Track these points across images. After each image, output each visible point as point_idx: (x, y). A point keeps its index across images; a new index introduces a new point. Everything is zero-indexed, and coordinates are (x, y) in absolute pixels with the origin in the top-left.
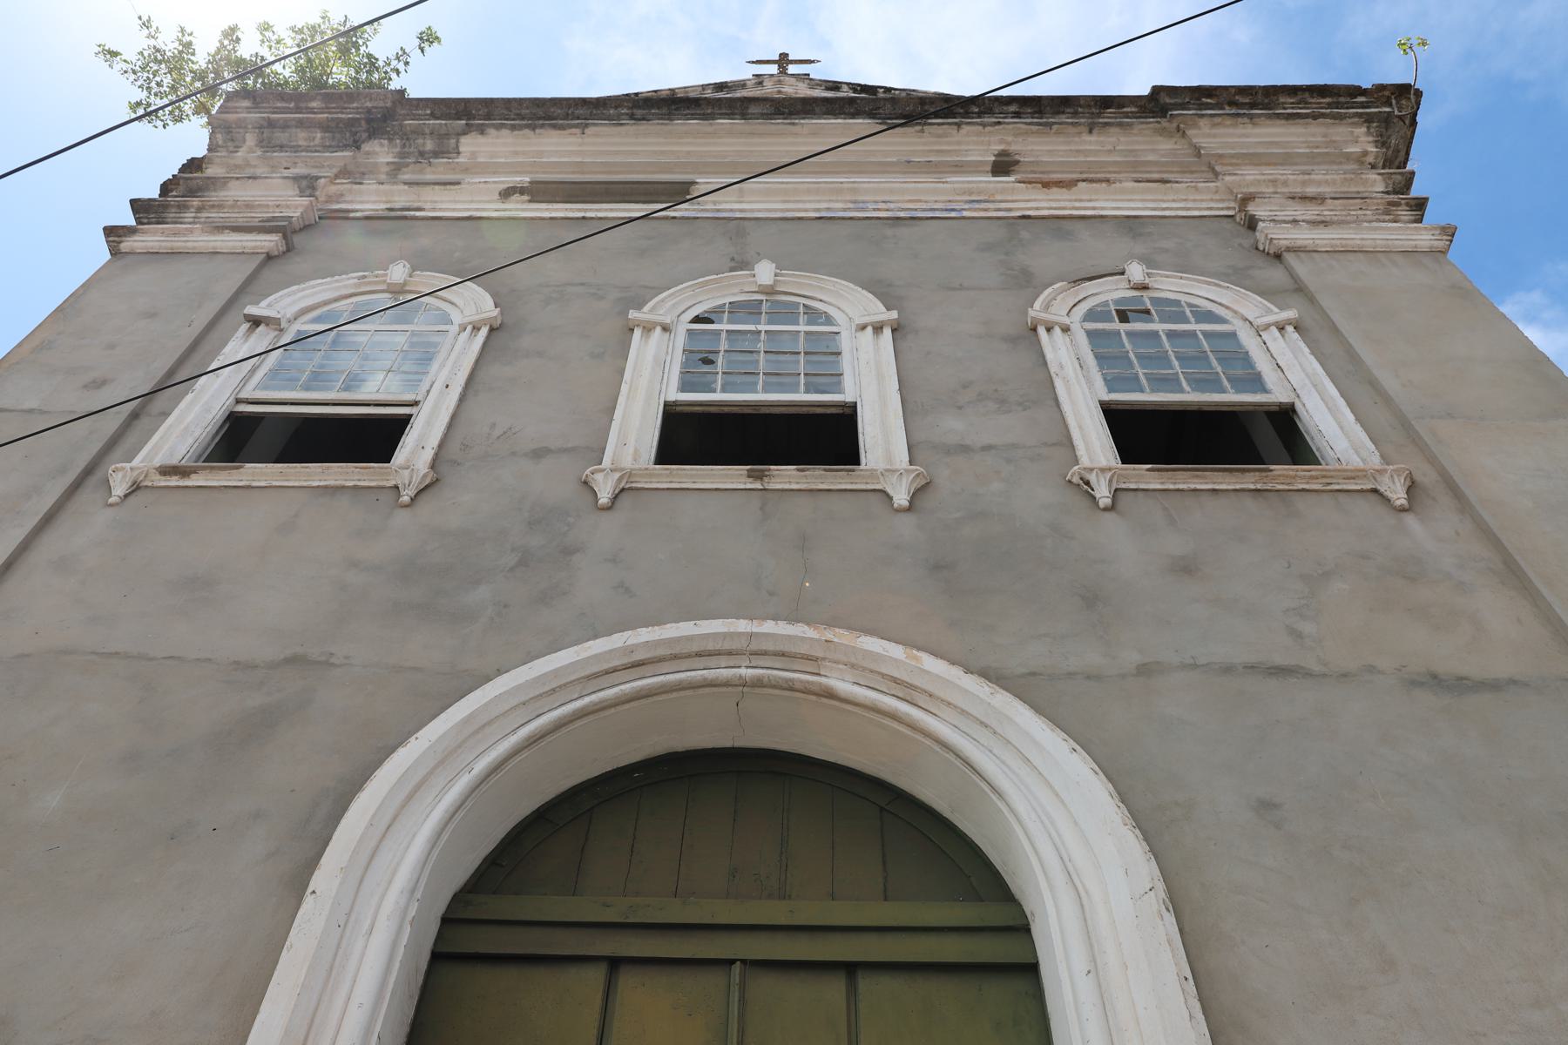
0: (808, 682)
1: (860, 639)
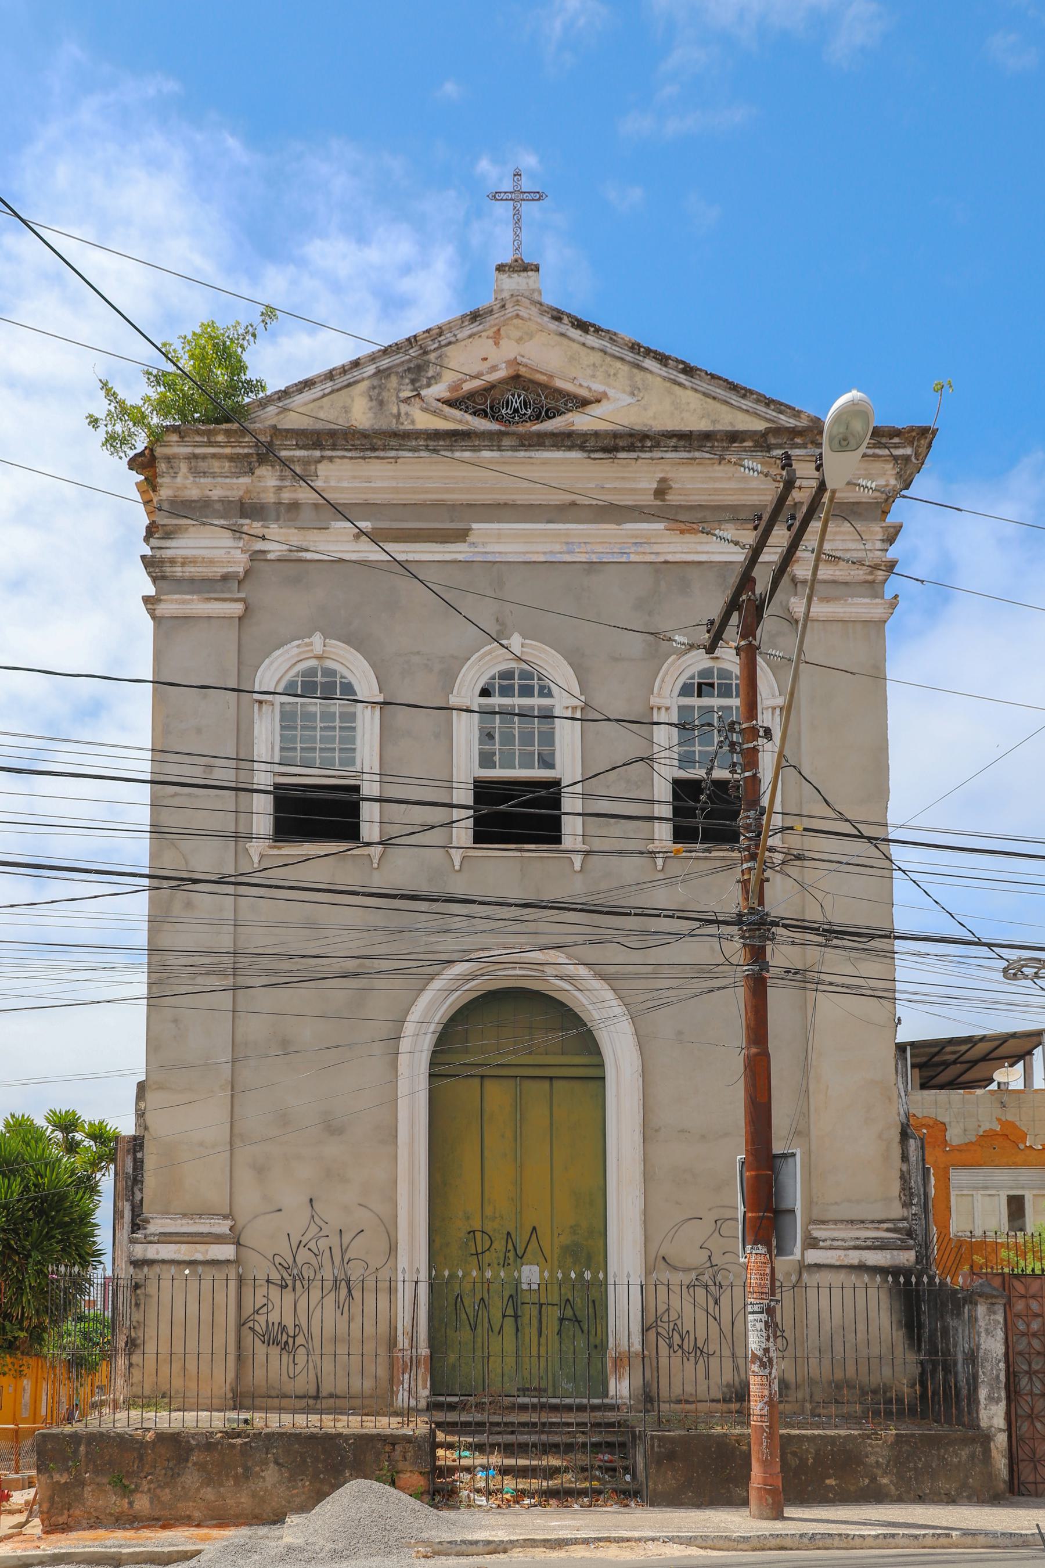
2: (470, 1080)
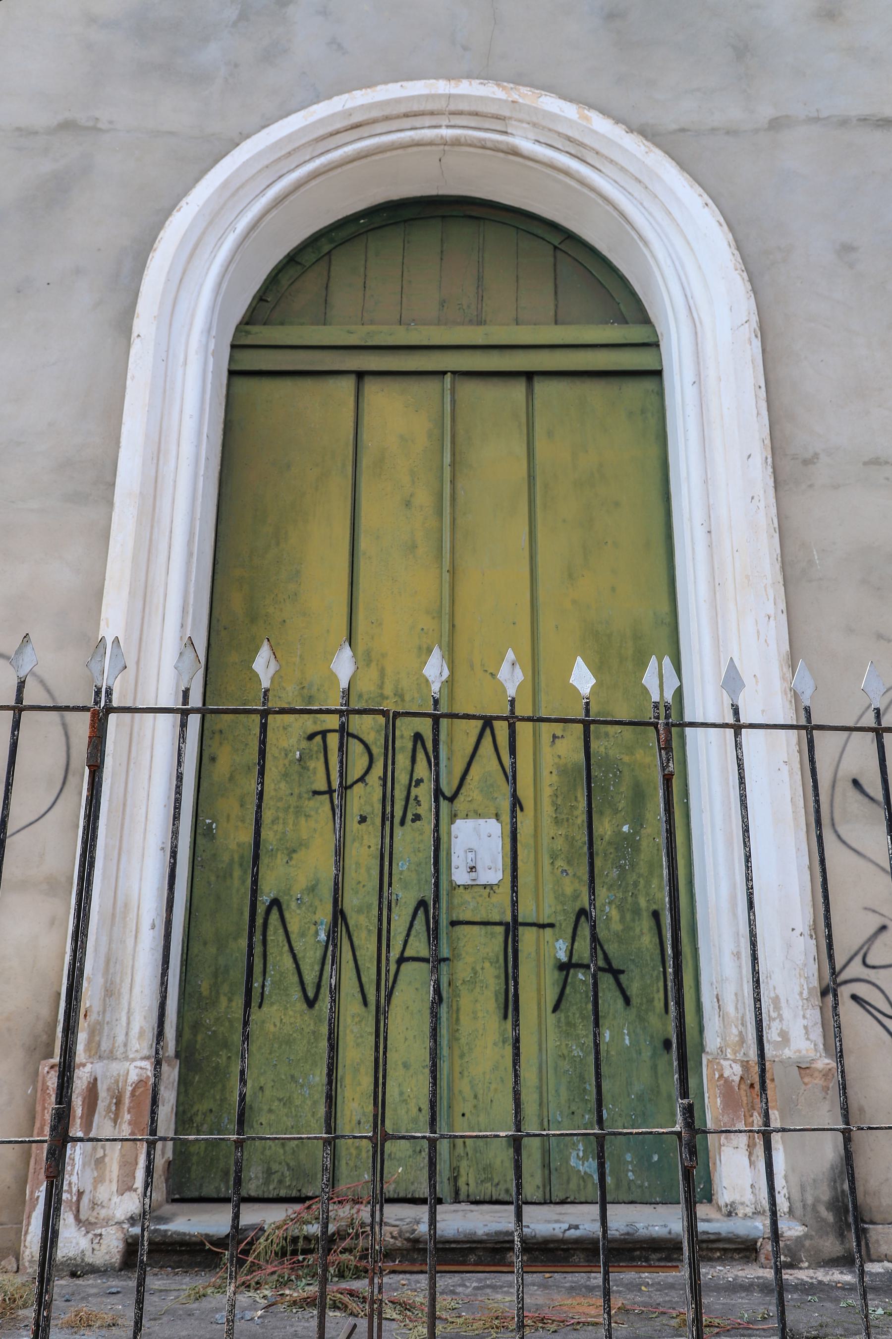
0: (498, 142)
1: (541, 99)
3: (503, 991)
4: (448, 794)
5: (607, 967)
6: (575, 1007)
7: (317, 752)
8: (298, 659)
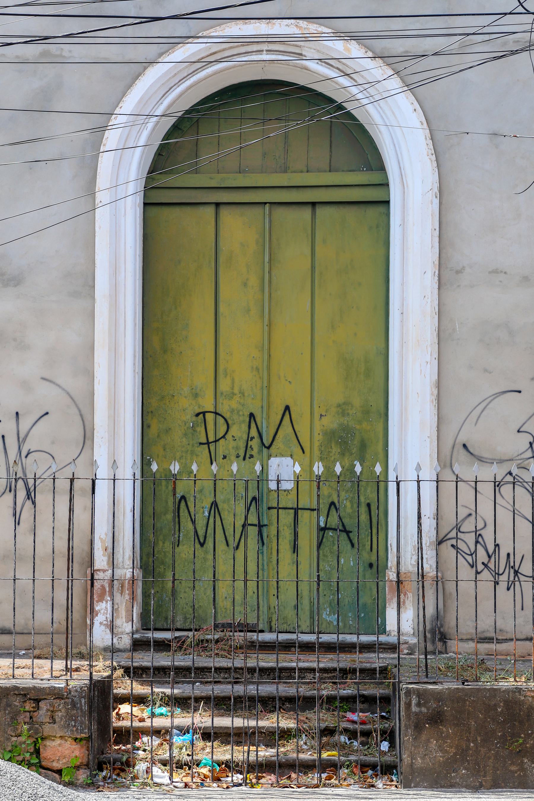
2: (201, 209)
3: (293, 540)
4: (267, 445)
5: (343, 529)
6: (327, 548)
7: (201, 423)
8: (189, 373)
